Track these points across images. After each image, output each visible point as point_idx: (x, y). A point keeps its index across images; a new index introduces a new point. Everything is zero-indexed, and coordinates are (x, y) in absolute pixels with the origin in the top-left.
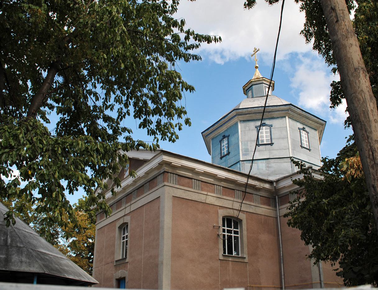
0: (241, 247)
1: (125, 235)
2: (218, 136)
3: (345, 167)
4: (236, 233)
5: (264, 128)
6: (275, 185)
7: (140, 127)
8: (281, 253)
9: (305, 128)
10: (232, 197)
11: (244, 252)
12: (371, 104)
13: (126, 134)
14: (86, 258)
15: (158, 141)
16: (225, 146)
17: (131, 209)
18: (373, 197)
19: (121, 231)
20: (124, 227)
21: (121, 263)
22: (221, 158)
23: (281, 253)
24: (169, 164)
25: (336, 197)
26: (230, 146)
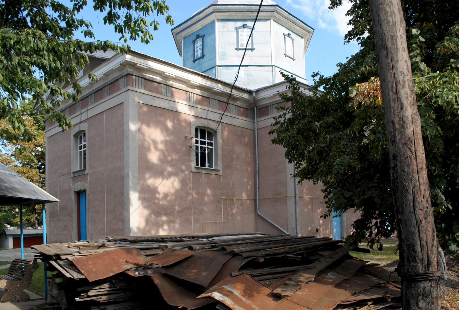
0: (215, 159)
1: (82, 144)
2: (191, 35)
3: (355, 93)
4: (210, 144)
6: (254, 96)
7: (105, 23)
8: (257, 166)
9: (290, 35)
10: (207, 106)
11: (218, 164)
12: (401, 29)
13: (84, 28)
14: (35, 168)
15: (125, 41)
16: (199, 47)
17: (88, 115)
18: (391, 133)
19: (77, 140)
20: (80, 136)
21: (79, 174)
22: (194, 61)
23: (257, 166)
24: (133, 65)
25: (330, 119)
26: (204, 47)
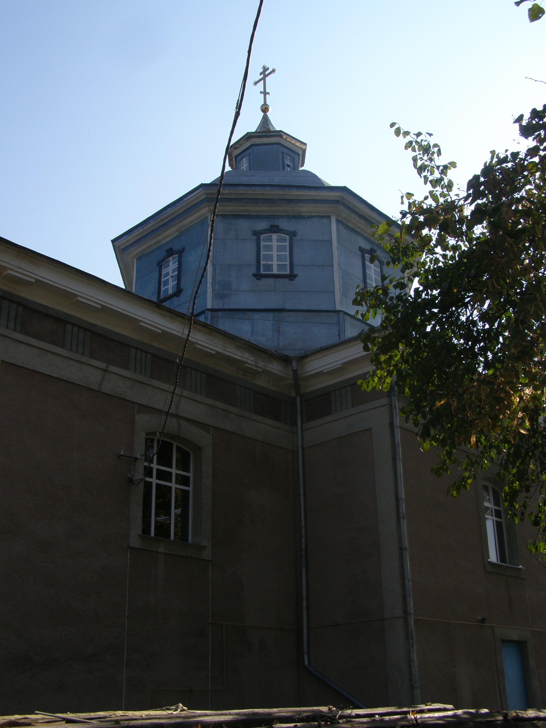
2: (154, 250)
4: (184, 480)
5: (275, 236)
8: (304, 540)
9: (375, 251)
16: (171, 274)
23: (304, 540)
